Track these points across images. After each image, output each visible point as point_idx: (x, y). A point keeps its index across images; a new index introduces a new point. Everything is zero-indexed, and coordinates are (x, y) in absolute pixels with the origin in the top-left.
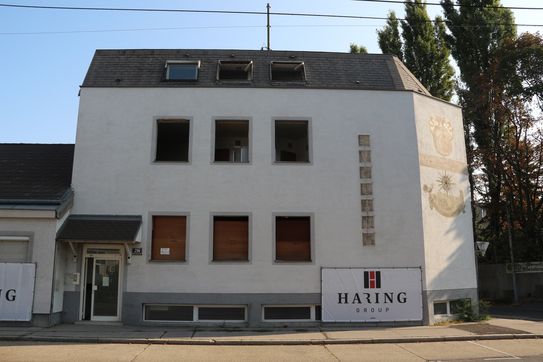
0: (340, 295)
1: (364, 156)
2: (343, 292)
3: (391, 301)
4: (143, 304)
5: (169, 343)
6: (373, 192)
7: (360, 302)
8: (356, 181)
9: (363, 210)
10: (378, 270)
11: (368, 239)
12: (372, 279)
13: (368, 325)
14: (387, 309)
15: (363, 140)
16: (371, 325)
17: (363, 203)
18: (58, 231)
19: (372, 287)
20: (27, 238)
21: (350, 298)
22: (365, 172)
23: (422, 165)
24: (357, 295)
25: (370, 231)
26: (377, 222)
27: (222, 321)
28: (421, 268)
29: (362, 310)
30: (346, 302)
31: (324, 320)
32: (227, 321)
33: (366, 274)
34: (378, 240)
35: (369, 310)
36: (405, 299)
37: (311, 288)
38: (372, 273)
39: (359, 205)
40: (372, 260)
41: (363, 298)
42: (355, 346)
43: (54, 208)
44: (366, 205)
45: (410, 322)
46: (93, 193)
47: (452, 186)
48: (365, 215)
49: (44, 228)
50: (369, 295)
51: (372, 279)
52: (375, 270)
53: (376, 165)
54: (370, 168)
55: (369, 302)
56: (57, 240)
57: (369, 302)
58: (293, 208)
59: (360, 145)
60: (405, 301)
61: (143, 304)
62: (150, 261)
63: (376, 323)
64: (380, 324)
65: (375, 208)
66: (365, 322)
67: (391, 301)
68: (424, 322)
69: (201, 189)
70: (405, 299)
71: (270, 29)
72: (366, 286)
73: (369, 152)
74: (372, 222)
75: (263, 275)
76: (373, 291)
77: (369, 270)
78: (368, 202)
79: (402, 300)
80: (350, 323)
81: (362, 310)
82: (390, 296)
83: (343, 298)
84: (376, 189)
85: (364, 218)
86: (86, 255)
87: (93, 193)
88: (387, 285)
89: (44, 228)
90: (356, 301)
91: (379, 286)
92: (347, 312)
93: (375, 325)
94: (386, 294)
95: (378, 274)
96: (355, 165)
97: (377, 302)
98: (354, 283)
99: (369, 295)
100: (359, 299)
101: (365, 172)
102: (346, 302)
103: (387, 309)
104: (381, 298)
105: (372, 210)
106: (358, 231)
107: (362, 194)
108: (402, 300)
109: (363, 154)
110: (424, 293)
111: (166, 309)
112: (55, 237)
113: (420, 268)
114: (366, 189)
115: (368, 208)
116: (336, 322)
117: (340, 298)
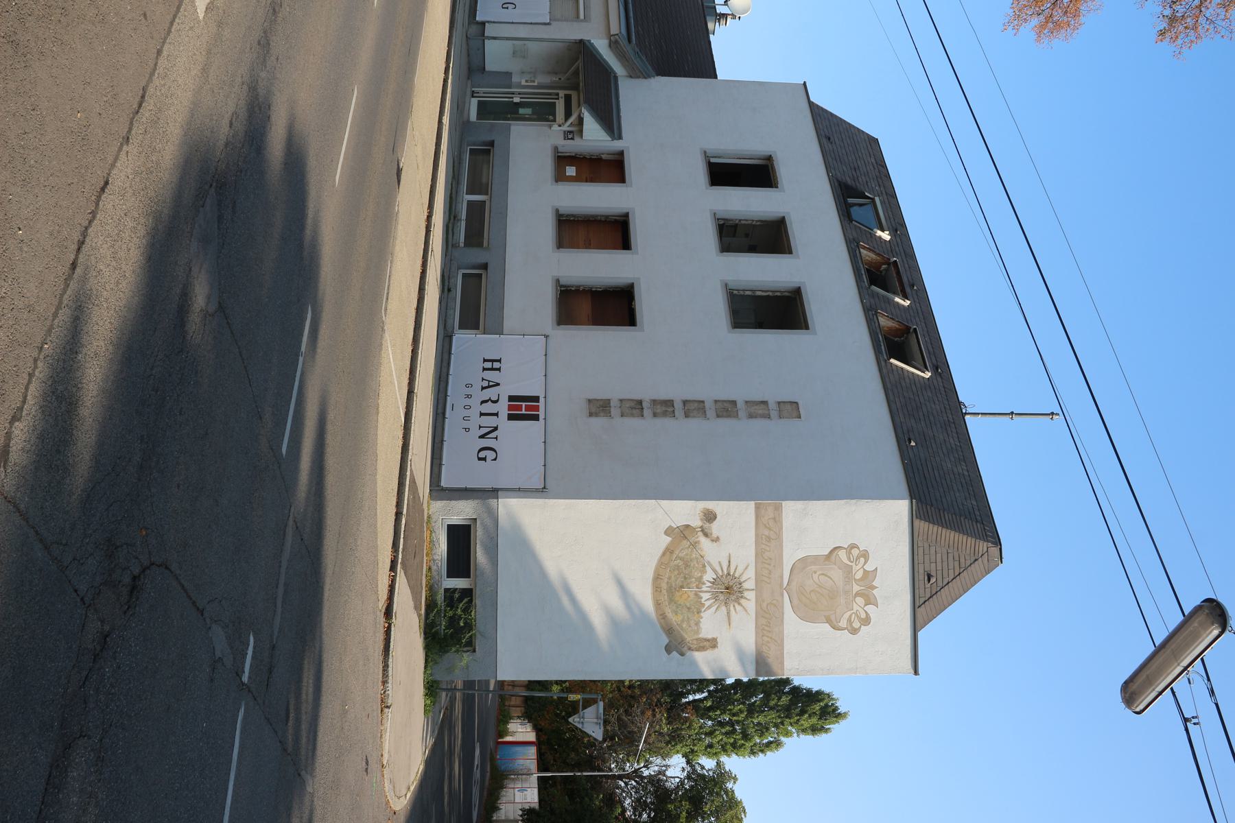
0: (499, 361)
1: (759, 409)
2: (503, 366)
3: (482, 437)
4: (485, 267)
5: (445, 81)
6: (690, 420)
7: (483, 388)
8: (709, 392)
9: (654, 402)
10: (542, 417)
11: (599, 407)
12: (524, 408)
13: (441, 401)
14: (467, 430)
15: (790, 409)
16: (440, 406)
17: (669, 403)
18: (592, 45)
19: (510, 408)
20: (582, 17)
21: (492, 376)
22: (727, 409)
23: (757, 507)
24: (498, 384)
25: (615, 411)
26: (633, 422)
27: (464, 217)
28: (542, 491)
29: (469, 391)
30: (484, 369)
31: (443, 484)
32: (463, 224)
33: (536, 399)
34: (598, 422)
35: (468, 401)
36: (484, 459)
37: (511, 316)
38: (537, 408)
39: (663, 395)
40: (557, 410)
41: (491, 393)
42: (419, 262)
43: (624, 31)
44: (664, 408)
45: (440, 465)
46: (648, 101)
47: (724, 608)
48: (644, 404)
49: (599, 29)
50: (496, 402)
51: (524, 408)
52: (541, 413)
53: (741, 426)
54: (736, 416)
55: (483, 402)
56: (581, 41)
57: (483, 402)
58: (645, 304)
59: (779, 403)
60: (480, 459)
61: (485, 267)
62: (557, 210)
63: (444, 413)
64: (446, 356)
65: (659, 422)
66: (446, 395)
67: (482, 437)
68: (438, 490)
69: (672, 211)
70: (484, 459)
71: (1007, 418)
72: (511, 398)
73: (768, 417)
74: (632, 415)
75: (532, 265)
76: (503, 408)
77: (541, 404)
78: (670, 409)
79: (482, 455)
80: (448, 374)
81: (469, 391)
82: (493, 435)
83: (493, 364)
84: (695, 423)
85: (640, 402)
86: (562, 93)
87: (648, 101)
88: (509, 429)
89: (599, 29)
90: (485, 384)
91: (511, 417)
92: (466, 368)
93: (440, 411)
94: (496, 429)
95: (536, 418)
96: (740, 393)
97: (482, 414)
98: (516, 381)
99: (496, 402)
100: (489, 387)
101: (727, 409)
102: (484, 369)
103: (467, 430)
104: (490, 421)
105: (655, 415)
106: (614, 391)
107: (685, 402)
108: (482, 455)
109: (763, 406)
110: (494, 492)
111: (484, 180)
112: (585, 38)
113: (547, 337)
114: (693, 408)
115: (659, 409)
116: (450, 353)
117: (492, 361)
